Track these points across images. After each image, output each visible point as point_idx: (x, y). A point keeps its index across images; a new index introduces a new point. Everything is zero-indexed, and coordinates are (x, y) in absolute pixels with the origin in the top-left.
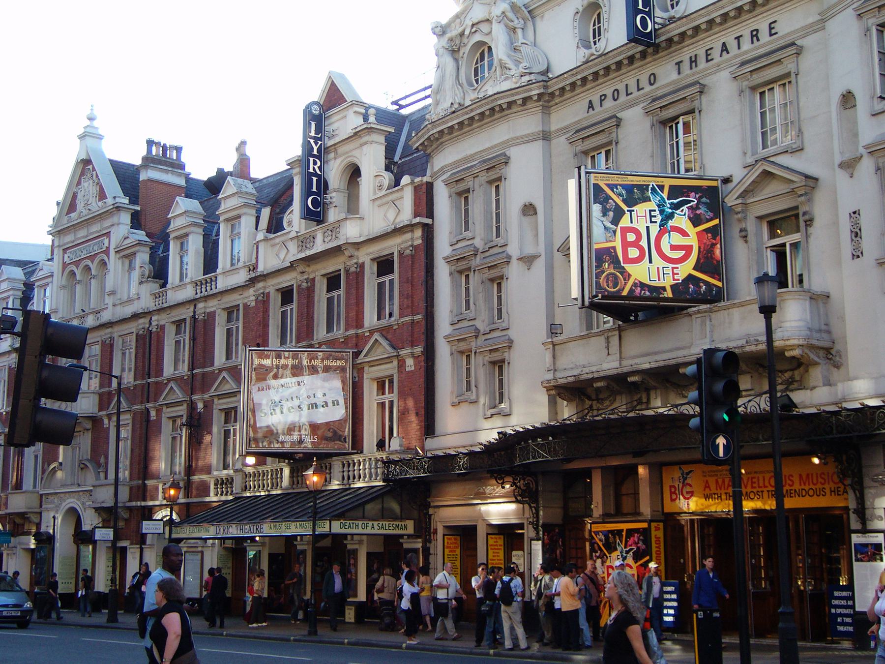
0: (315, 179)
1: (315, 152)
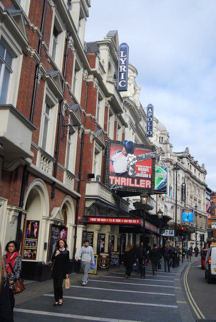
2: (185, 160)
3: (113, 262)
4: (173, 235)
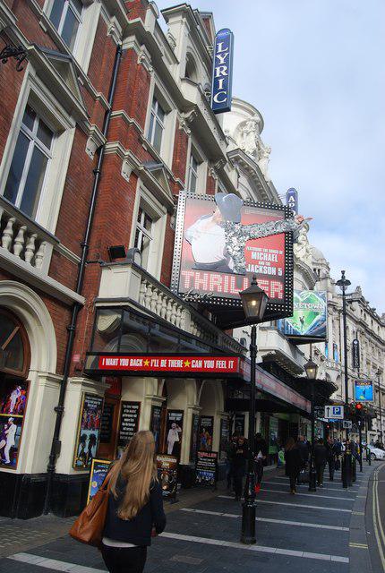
0: (221, 81)
2: (355, 305)
3: (201, 476)
4: (342, 416)
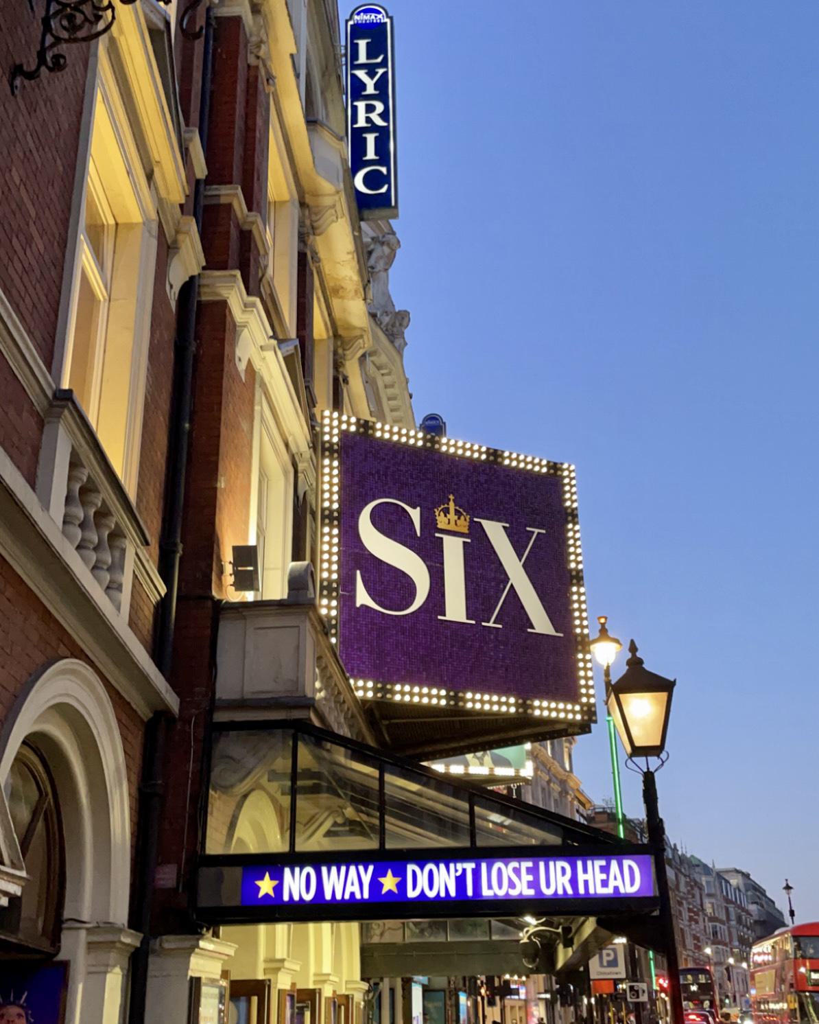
0: (371, 138)
1: (370, 90)
